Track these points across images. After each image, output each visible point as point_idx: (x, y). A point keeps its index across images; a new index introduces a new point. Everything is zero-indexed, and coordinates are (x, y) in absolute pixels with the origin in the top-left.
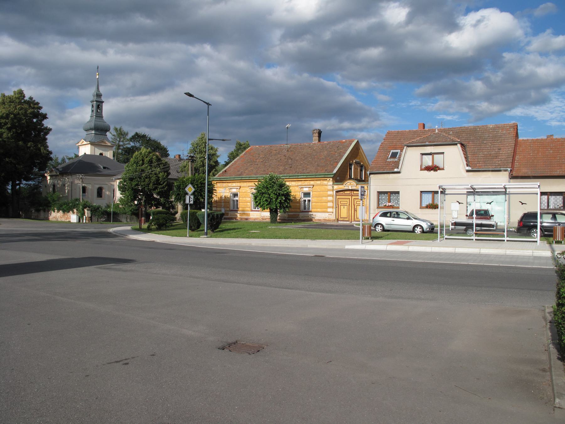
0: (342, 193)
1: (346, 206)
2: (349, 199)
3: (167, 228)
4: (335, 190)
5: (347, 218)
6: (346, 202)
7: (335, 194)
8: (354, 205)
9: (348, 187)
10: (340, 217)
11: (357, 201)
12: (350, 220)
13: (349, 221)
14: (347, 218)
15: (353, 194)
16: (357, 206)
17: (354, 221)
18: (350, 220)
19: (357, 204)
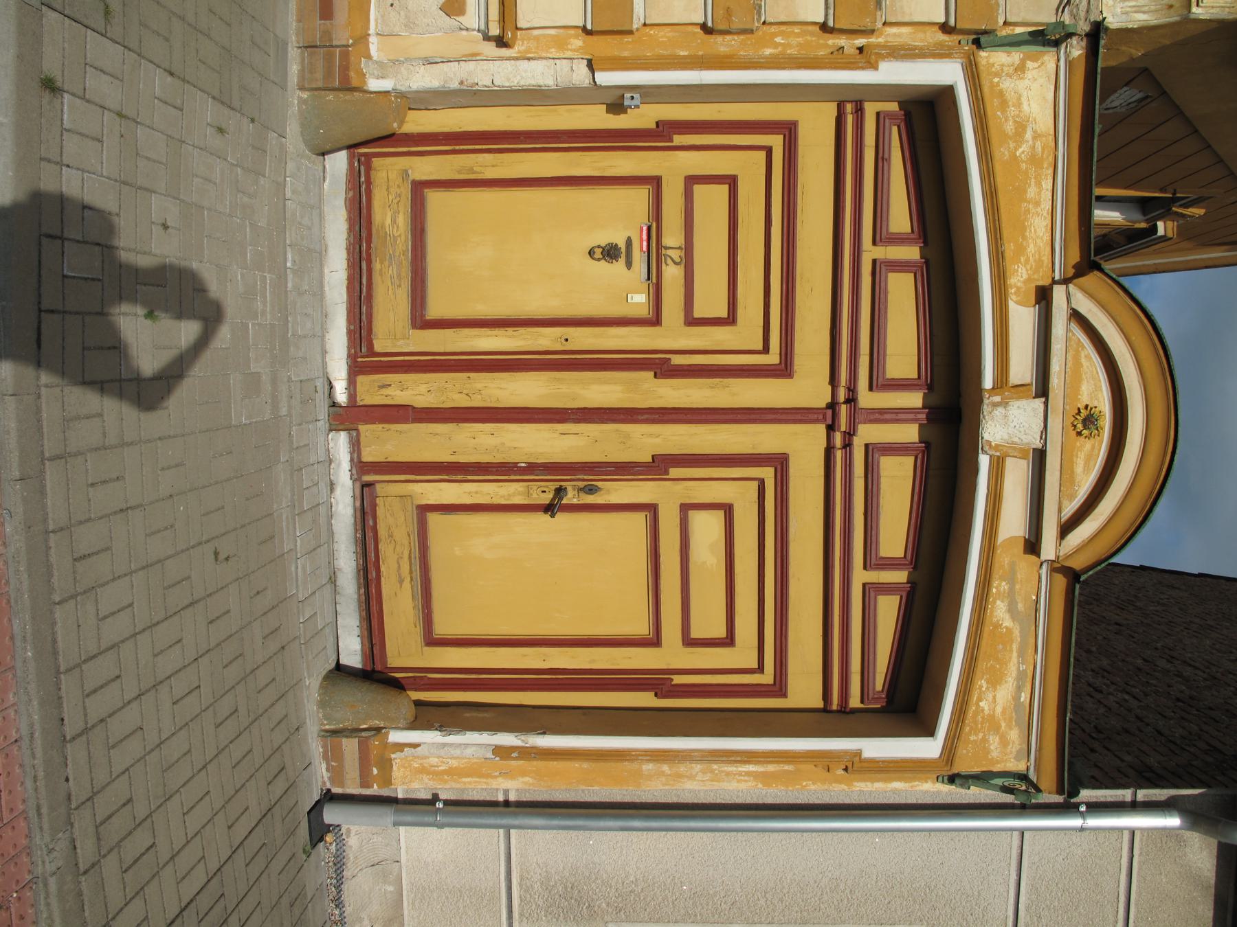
0: (900, 217)
1: (640, 300)
2: (784, 370)
3: (635, 417)
4: (973, 74)
5: (421, 321)
6: (711, 301)
7: (893, 73)
8: (660, 466)
9: (1022, 368)
10: (426, 167)
11: (731, 182)
12: (374, 391)
13: (356, 369)
14: (421, 321)
15: (868, 433)
16: (639, 520)
17: (361, 467)
18: (374, 391)
19: (685, 508)
